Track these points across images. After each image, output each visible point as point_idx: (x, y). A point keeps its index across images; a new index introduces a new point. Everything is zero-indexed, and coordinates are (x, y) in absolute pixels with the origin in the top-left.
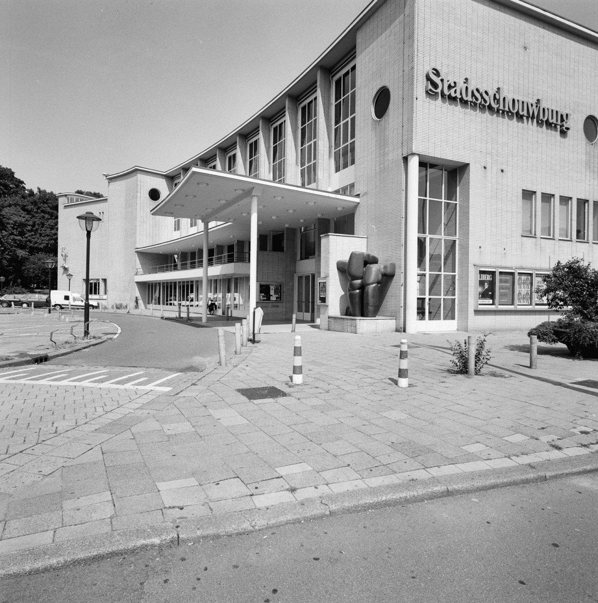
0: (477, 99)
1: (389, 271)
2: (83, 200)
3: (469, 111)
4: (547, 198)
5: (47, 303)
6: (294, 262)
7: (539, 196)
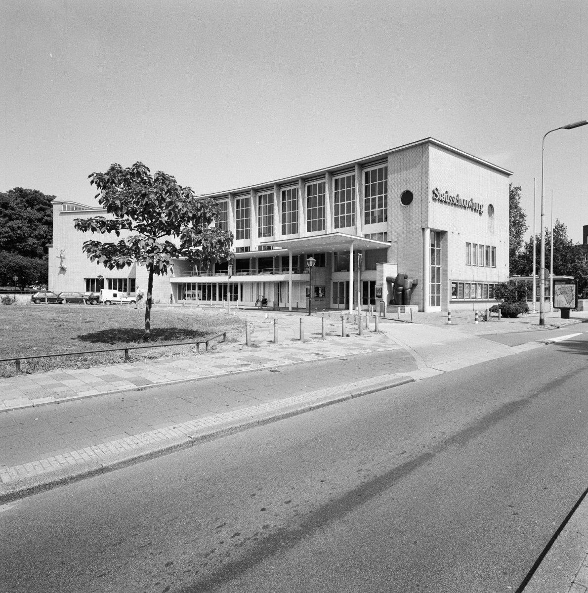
0: (451, 201)
1: (415, 283)
2: (83, 210)
3: (447, 206)
4: (475, 245)
5: (97, 299)
6: (330, 273)
7: (472, 245)
